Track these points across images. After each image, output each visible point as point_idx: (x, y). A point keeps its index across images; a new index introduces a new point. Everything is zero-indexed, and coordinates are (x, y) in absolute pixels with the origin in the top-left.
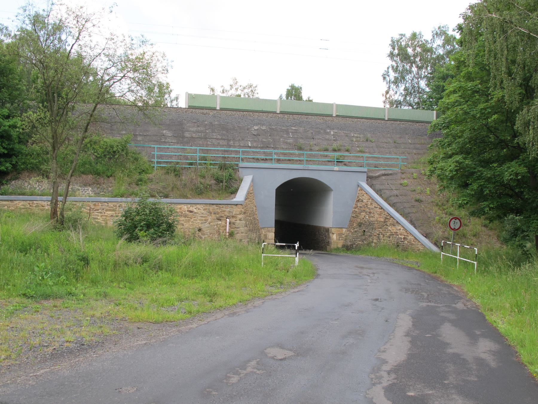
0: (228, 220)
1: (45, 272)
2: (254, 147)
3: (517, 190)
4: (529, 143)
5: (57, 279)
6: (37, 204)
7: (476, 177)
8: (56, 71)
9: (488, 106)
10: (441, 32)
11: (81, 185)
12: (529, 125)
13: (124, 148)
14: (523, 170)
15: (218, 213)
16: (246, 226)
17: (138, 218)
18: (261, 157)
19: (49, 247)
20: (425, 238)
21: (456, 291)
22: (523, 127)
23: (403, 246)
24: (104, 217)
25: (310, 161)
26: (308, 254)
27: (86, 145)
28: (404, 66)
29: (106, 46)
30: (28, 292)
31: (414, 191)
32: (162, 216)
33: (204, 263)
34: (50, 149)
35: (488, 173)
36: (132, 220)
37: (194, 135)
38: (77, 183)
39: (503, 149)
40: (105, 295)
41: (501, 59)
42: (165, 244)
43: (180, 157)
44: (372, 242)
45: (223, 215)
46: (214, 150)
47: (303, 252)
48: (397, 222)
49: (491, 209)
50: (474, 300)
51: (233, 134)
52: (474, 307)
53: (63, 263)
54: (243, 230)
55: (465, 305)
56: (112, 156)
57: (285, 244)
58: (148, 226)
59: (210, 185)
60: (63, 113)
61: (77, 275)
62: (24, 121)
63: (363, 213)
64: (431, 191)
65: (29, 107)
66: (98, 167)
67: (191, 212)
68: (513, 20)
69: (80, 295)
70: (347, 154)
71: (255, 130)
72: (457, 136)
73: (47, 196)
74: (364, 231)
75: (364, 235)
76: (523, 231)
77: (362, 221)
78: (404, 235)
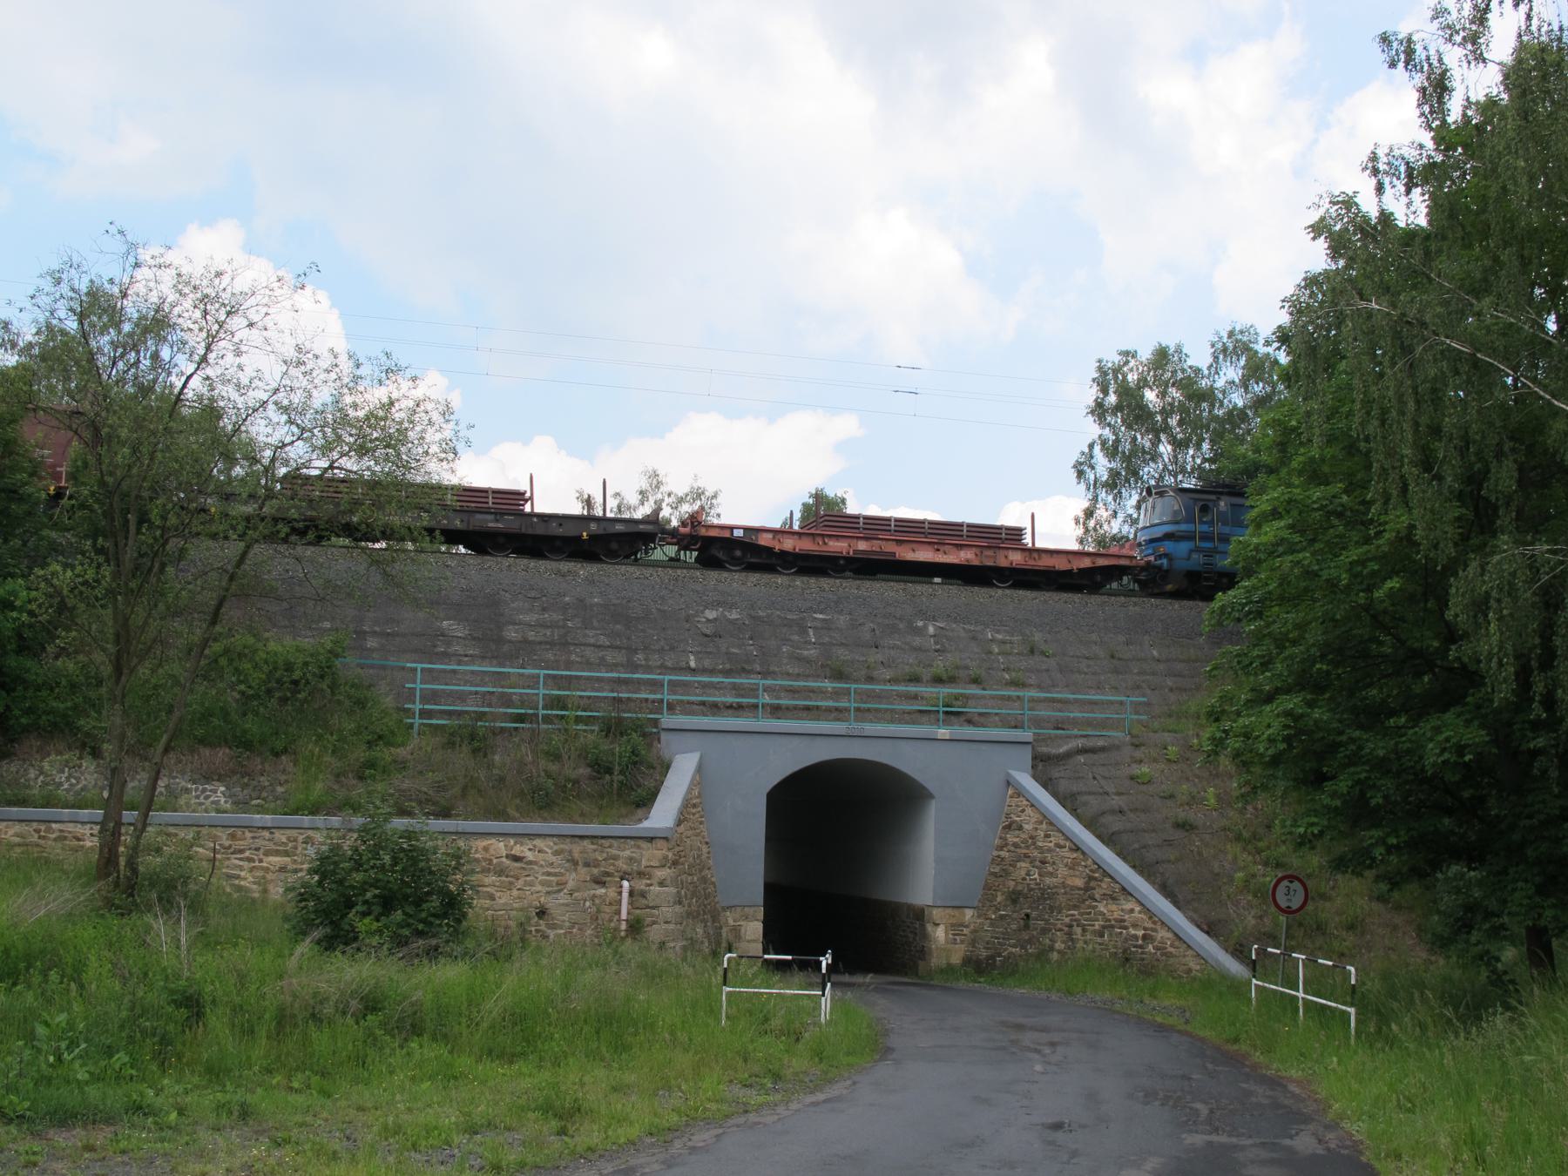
0: (626, 884)
1: (67, 1042)
2: (704, 671)
3: (1466, 794)
4: (1491, 660)
5: (102, 1063)
6: (61, 831)
7: (1346, 756)
8: (135, 450)
9: (1370, 556)
10: (1235, 346)
11: (195, 776)
12: (1488, 608)
13: (325, 671)
14: (1476, 736)
15: (596, 864)
16: (680, 903)
17: (358, 877)
18: (723, 699)
19: (85, 965)
20: (1206, 936)
21: (1294, 1095)
22: (1471, 614)
23: (1143, 959)
24: (259, 874)
25: (869, 710)
26: (860, 985)
27: (216, 661)
28: (1134, 439)
29: (284, 382)
30: (11, 1102)
31: (1172, 796)
32: (431, 873)
33: (549, 1015)
34: (107, 670)
35: (1378, 747)
36: (341, 882)
37: (531, 635)
38: (183, 773)
39: (1418, 675)
40: (245, 1113)
41: (1399, 422)
42: (436, 958)
43: (487, 697)
44: (1052, 948)
45: (611, 869)
46: (588, 678)
47: (846, 978)
48: (1124, 889)
49: (1390, 849)
50: (1346, 1125)
51: (643, 631)
52: (1346, 1148)
53: (124, 1014)
54: (669, 915)
55: (1320, 1141)
56: (289, 694)
57: (790, 957)
58: (387, 903)
59: (576, 782)
60: (150, 570)
61: (165, 1053)
62: (37, 590)
63: (1023, 865)
64: (1218, 797)
65: (55, 549)
66: (247, 726)
67: (517, 859)
68: (1428, 318)
69: (168, 1113)
70: (973, 690)
71: (708, 621)
72: (1288, 640)
73: (93, 808)
74: (1027, 915)
75: (1027, 927)
76: (1489, 915)
77: (1019, 888)
78: (1145, 929)
